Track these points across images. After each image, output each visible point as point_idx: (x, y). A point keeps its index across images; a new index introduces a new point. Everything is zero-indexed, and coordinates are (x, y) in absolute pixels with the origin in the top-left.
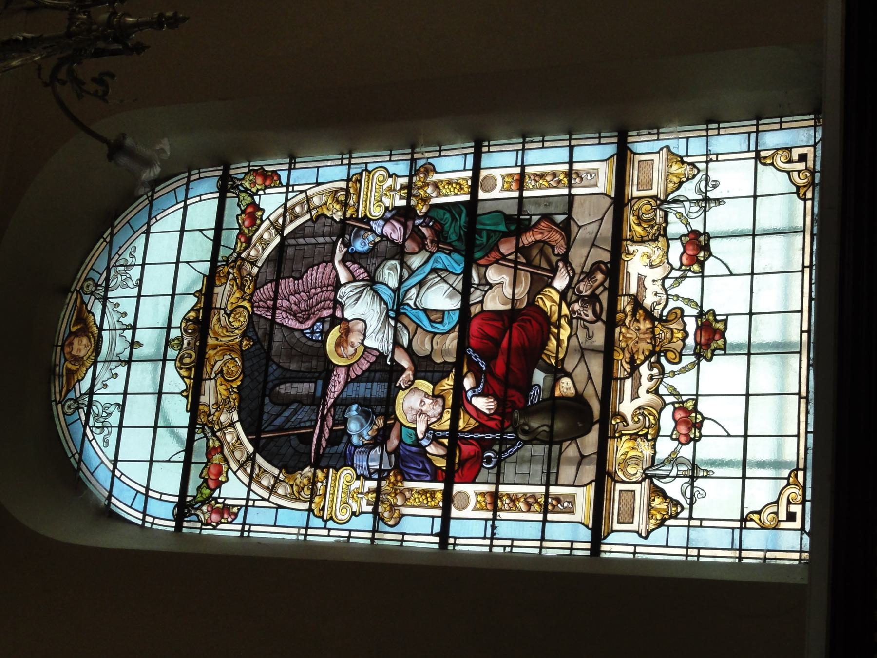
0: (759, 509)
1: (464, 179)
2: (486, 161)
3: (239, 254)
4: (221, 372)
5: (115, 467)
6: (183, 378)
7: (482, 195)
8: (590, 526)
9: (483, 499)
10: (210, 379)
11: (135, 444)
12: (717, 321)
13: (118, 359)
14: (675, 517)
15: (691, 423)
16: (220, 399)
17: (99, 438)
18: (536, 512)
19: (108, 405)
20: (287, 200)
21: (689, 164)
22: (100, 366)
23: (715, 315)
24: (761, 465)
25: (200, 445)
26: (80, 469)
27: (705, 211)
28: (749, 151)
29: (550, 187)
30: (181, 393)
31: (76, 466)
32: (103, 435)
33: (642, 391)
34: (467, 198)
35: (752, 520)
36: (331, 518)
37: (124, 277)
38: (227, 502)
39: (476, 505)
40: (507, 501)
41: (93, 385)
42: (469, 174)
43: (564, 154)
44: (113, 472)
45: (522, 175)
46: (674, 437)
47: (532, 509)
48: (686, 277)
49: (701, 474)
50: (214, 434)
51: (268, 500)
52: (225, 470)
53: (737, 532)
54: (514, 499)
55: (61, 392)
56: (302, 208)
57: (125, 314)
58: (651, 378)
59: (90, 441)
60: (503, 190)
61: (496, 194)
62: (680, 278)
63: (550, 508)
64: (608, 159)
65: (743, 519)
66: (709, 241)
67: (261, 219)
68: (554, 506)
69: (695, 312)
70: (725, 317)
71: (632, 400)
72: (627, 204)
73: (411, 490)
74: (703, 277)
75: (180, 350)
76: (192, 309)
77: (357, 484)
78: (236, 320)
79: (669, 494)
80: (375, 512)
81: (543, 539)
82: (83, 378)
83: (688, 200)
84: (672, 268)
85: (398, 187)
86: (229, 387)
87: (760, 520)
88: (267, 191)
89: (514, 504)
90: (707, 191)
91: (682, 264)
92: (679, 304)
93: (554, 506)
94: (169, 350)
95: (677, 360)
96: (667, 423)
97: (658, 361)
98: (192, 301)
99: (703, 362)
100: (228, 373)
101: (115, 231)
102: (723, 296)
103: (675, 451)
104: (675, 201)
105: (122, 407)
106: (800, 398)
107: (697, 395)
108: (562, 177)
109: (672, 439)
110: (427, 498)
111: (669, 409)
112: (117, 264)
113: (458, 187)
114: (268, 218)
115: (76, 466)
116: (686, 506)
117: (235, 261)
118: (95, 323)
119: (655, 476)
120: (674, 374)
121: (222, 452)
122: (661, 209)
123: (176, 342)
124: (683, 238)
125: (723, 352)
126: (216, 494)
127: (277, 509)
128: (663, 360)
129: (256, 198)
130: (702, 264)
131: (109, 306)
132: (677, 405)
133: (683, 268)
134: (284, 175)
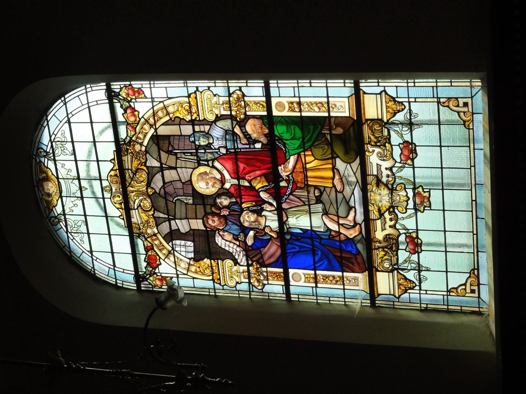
3: (131, 138)
4: (140, 205)
5: (92, 255)
6: (118, 208)
12: (425, 192)
18: (324, 112)
21: (399, 102)
24: (453, 245)
30: (110, 161)
31: (69, 254)
33: (387, 226)
35: (453, 292)
36: (225, 285)
38: (163, 275)
40: (307, 106)
48: (404, 167)
51: (187, 274)
56: (163, 112)
58: (391, 220)
62: (401, 167)
65: (449, 291)
69: (412, 187)
74: (414, 168)
75: (112, 193)
76: (112, 170)
80: (250, 283)
81: (327, 87)
82: (56, 205)
84: (396, 162)
85: (221, 103)
87: (457, 292)
88: (137, 100)
91: (401, 160)
94: (105, 193)
97: (394, 211)
98: (110, 165)
99: (419, 213)
100: (144, 206)
103: (409, 257)
104: (393, 123)
106: (474, 234)
108: (338, 279)
109: (406, 251)
115: (69, 254)
116: (418, 284)
118: (52, 174)
120: (403, 218)
121: (153, 249)
122: (385, 128)
126: (157, 271)
128: (396, 210)
130: (413, 160)
133: (402, 162)
134: (147, 92)
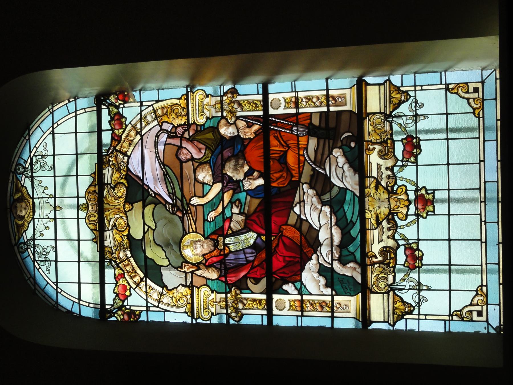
0: (460, 309)
1: (258, 101)
2: (271, 88)
4: (115, 225)
5: (57, 287)
6: (92, 230)
7: (272, 112)
8: (361, 320)
9: (294, 304)
10: (109, 230)
11: (68, 272)
12: (428, 194)
13: (47, 217)
14: (411, 313)
15: (415, 259)
16: (117, 243)
17: (44, 268)
18: (328, 312)
19: (46, 247)
20: (141, 111)
22: (36, 221)
23: (426, 190)
25: (110, 274)
26: (35, 289)
27: (416, 123)
28: (441, 84)
29: (315, 106)
31: (33, 288)
32: (46, 266)
33: (384, 237)
34: (261, 113)
36: (199, 317)
37: (42, 164)
38: (132, 308)
39: (290, 308)
40: (309, 305)
41: (34, 234)
42: (261, 97)
43: (322, 84)
44: (56, 290)
45: (297, 98)
46: (406, 265)
47: (324, 309)
49: (424, 288)
50: (118, 266)
51: (158, 307)
52: (128, 288)
53: (447, 322)
54: (312, 304)
55: (15, 239)
57: (46, 188)
59: (38, 270)
60: (285, 108)
61: (281, 111)
63: (335, 308)
64: (351, 88)
65: (450, 315)
66: (419, 142)
67: (125, 124)
68: (338, 308)
69: (414, 188)
70: (432, 191)
71: (379, 242)
72: (366, 118)
73: (246, 299)
74: (417, 166)
76: (91, 185)
77: (212, 296)
78: (119, 191)
79: (405, 300)
82: (27, 230)
83: (405, 116)
84: (398, 160)
86: (121, 235)
89: (313, 306)
90: (416, 109)
91: (404, 157)
92: (404, 183)
93: (338, 308)
94: (81, 212)
95: (404, 218)
96: (401, 257)
99: (421, 219)
101: (31, 132)
102: (430, 178)
105: (56, 248)
106: (482, 242)
107: (419, 240)
110: (257, 304)
111: (402, 248)
112: (36, 154)
113: (254, 105)
114: (130, 123)
115: (33, 288)
117: (112, 153)
118: (28, 193)
119: (396, 289)
120: (403, 227)
123: (84, 206)
124: (403, 141)
125: (433, 213)
126: (125, 303)
127: (164, 312)
128: (396, 217)
129: (121, 110)
131: (36, 183)
132: (406, 246)
